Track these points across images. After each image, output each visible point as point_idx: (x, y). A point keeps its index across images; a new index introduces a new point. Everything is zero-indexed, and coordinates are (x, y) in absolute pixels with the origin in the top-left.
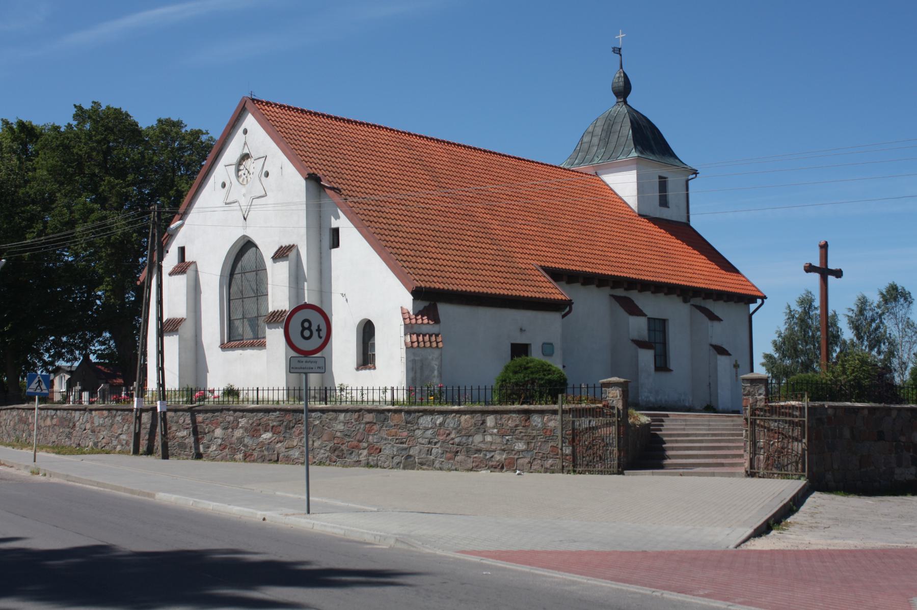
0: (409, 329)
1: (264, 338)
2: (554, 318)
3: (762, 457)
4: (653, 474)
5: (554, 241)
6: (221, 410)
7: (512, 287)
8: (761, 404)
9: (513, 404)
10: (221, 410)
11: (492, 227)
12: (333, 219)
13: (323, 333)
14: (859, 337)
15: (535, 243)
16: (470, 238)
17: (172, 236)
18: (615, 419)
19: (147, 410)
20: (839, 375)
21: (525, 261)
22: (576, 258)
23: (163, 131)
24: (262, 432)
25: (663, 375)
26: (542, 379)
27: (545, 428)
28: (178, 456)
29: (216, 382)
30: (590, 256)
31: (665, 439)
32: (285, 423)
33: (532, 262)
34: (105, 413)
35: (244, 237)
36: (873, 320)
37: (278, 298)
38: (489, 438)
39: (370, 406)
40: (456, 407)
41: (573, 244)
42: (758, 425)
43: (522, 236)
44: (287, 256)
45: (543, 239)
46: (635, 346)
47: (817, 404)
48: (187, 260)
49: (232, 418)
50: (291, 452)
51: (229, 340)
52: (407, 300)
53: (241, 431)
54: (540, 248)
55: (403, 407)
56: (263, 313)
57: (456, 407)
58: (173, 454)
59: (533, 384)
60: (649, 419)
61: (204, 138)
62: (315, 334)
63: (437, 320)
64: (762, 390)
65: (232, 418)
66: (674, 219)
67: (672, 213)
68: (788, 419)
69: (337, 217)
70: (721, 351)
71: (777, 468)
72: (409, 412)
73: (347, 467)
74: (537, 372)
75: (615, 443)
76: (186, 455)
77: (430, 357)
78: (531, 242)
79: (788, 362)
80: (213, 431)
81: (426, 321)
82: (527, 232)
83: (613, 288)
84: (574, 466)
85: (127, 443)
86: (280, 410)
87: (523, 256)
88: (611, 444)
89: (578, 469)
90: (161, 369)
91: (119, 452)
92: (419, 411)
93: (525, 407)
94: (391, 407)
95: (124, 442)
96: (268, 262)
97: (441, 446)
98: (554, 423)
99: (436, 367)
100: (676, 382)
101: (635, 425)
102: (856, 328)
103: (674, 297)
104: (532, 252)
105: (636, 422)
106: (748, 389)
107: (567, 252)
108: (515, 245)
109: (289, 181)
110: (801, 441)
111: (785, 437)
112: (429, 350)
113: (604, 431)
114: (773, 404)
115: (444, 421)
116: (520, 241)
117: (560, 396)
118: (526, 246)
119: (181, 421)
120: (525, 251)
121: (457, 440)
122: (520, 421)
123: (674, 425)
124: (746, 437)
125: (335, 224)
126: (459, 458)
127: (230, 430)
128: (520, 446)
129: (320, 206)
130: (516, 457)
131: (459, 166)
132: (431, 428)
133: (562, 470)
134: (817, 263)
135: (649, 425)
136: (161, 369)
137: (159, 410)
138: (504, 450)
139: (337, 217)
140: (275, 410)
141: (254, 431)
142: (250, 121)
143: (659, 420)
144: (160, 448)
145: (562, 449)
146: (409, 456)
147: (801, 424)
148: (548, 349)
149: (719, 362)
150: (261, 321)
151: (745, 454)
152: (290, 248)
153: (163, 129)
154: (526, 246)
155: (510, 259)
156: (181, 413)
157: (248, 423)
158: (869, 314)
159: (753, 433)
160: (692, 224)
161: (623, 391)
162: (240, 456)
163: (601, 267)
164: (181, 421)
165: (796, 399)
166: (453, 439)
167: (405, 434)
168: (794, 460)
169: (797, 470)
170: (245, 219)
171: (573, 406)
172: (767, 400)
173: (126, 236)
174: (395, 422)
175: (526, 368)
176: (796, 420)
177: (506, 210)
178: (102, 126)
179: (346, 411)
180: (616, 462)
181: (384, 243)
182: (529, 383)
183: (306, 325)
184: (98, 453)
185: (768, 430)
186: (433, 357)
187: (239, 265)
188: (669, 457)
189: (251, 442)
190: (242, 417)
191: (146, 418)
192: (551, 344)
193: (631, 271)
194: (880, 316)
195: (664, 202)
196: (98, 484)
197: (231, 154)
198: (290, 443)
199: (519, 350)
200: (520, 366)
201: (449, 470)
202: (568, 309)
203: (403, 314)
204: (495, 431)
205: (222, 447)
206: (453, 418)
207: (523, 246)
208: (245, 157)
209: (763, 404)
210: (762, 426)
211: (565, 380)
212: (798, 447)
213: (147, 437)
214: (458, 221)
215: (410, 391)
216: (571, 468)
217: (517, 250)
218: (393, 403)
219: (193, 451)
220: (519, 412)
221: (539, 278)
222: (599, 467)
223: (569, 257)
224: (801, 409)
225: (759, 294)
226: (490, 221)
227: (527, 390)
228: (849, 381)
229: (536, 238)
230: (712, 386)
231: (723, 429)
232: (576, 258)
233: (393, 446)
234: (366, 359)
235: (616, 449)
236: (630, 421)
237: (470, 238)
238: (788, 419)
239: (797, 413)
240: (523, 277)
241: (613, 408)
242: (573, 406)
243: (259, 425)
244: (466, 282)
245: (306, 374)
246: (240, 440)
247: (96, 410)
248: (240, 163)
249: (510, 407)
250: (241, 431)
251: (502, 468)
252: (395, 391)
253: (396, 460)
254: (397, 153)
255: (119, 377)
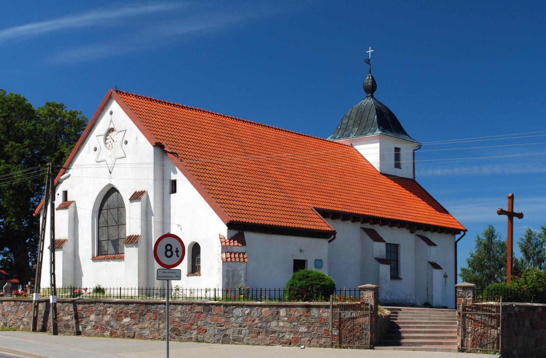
0: (225, 249)
1: (123, 253)
2: (323, 243)
3: (469, 339)
4: (394, 349)
5: (323, 190)
6: (95, 303)
7: (295, 221)
8: (470, 303)
9: (298, 301)
10: (95, 303)
11: (281, 180)
12: (172, 174)
13: (180, 254)
14: (528, 258)
15: (310, 192)
16: (266, 188)
17: (59, 183)
18: (369, 312)
19: (42, 302)
20: (522, 285)
21: (303, 204)
22: (338, 203)
23: (50, 110)
24: (123, 317)
25: (396, 282)
26: (318, 284)
27: (320, 318)
28: (64, 333)
29: (88, 283)
30: (347, 201)
31: (400, 325)
32: (139, 312)
33: (308, 205)
34: (13, 303)
35: (110, 184)
36: (537, 246)
37: (133, 225)
38: (281, 324)
39: (199, 301)
40: (259, 303)
41: (336, 193)
42: (468, 317)
43: (302, 187)
44: (140, 198)
45: (316, 189)
46: (378, 262)
47: (508, 304)
48: (69, 200)
49: (102, 308)
50: (143, 332)
51: (99, 254)
52: (223, 230)
53: (109, 317)
54: (314, 195)
55: (222, 302)
56: (122, 236)
57: (259, 303)
58: (60, 332)
59: (312, 288)
60: (389, 312)
61: (78, 116)
62: (175, 254)
63: (244, 243)
64: (471, 294)
65: (102, 308)
66: (405, 176)
67: (405, 172)
68: (488, 313)
69: (175, 173)
70: (436, 266)
71: (480, 346)
72: (226, 306)
73: (182, 342)
74: (315, 280)
75: (369, 328)
76: (70, 332)
77: (239, 269)
78: (308, 191)
79: (477, 274)
80: (89, 317)
81: (236, 244)
82: (305, 184)
83: (362, 223)
84: (340, 343)
85: (28, 324)
86: (136, 303)
87: (302, 200)
88: (366, 329)
89: (342, 346)
90: (53, 274)
91: (22, 330)
92: (233, 305)
93: (307, 303)
94: (214, 302)
95: (26, 323)
96: (127, 202)
97: (248, 329)
98: (326, 314)
99: (243, 275)
100: (406, 286)
101: (382, 316)
102: (525, 251)
103: (404, 229)
104: (308, 198)
105: (383, 315)
106: (461, 293)
107: (332, 198)
108: (297, 193)
109: (142, 148)
110: (497, 329)
111: (486, 325)
112: (238, 264)
113: (361, 320)
114: (478, 303)
115: (251, 312)
116: (300, 190)
117: (331, 296)
118: (304, 194)
119: (66, 309)
120: (303, 197)
121: (259, 325)
122: (303, 312)
123: (406, 316)
124: (459, 325)
125: (173, 177)
126: (260, 337)
127: (101, 316)
128: (303, 329)
129: (163, 165)
130: (300, 336)
131: (258, 139)
132: (241, 316)
133: (332, 346)
134: (506, 209)
135: (390, 316)
136: (53, 274)
137: (51, 302)
138: (292, 332)
139: (175, 173)
140: (132, 303)
141: (118, 317)
142: (114, 106)
143: (395, 313)
144: (52, 328)
145: (332, 332)
146: (226, 335)
147: (497, 317)
148: (318, 263)
149: (434, 274)
150: (121, 242)
151: (458, 337)
152: (142, 193)
153: (50, 109)
154: (304, 194)
155: (293, 203)
156: (66, 304)
157: (113, 311)
158: (533, 241)
159: (464, 323)
160: (416, 180)
161: (375, 293)
162: (108, 333)
163: (354, 208)
164: (66, 309)
165: (494, 300)
166: (256, 324)
167: (224, 320)
168: (491, 341)
169: (493, 348)
170: (110, 173)
171: (340, 303)
172: (474, 300)
173: (24, 183)
174: (216, 312)
175: (307, 277)
176: (494, 314)
177: (290, 169)
178: (7, 106)
179: (183, 304)
180: (369, 341)
181: (208, 191)
182: (308, 287)
183: (169, 248)
184: (8, 330)
185: (474, 321)
186: (241, 269)
187: (106, 204)
188: (404, 338)
189: (115, 324)
190: (109, 307)
191: (41, 307)
192: (321, 260)
193: (375, 211)
194: (541, 244)
195: (398, 166)
196: (14, 352)
197: (101, 127)
198: (143, 325)
199: (299, 265)
200: (303, 276)
201: (254, 344)
202: (333, 237)
203: (221, 239)
204: (286, 319)
205: (95, 327)
206: (257, 310)
207: (302, 194)
208: (111, 130)
209: (471, 303)
210: (470, 318)
211: (334, 285)
212: (495, 333)
213: (42, 319)
214: (258, 176)
215: (226, 290)
216: (338, 344)
217: (298, 196)
218: (215, 299)
219: (75, 330)
220: (302, 306)
221: (313, 216)
222: (357, 344)
223: (334, 202)
224: (498, 307)
225: (462, 228)
226: (280, 177)
227: (308, 291)
228: (529, 289)
229: (311, 188)
230: (429, 290)
231: (439, 319)
232: (338, 203)
233: (215, 328)
234: (195, 269)
235: (369, 332)
236: (379, 313)
237: (266, 188)
238: (488, 313)
239: (495, 310)
240: (303, 215)
241: (368, 304)
242: (340, 303)
243: (121, 312)
244: (264, 218)
245: (168, 280)
246: (108, 323)
247: (5, 301)
248: (107, 135)
249: (296, 303)
250: (109, 317)
251: (290, 344)
252: (217, 291)
253: (217, 337)
254: (216, 129)
255: (15, 278)
